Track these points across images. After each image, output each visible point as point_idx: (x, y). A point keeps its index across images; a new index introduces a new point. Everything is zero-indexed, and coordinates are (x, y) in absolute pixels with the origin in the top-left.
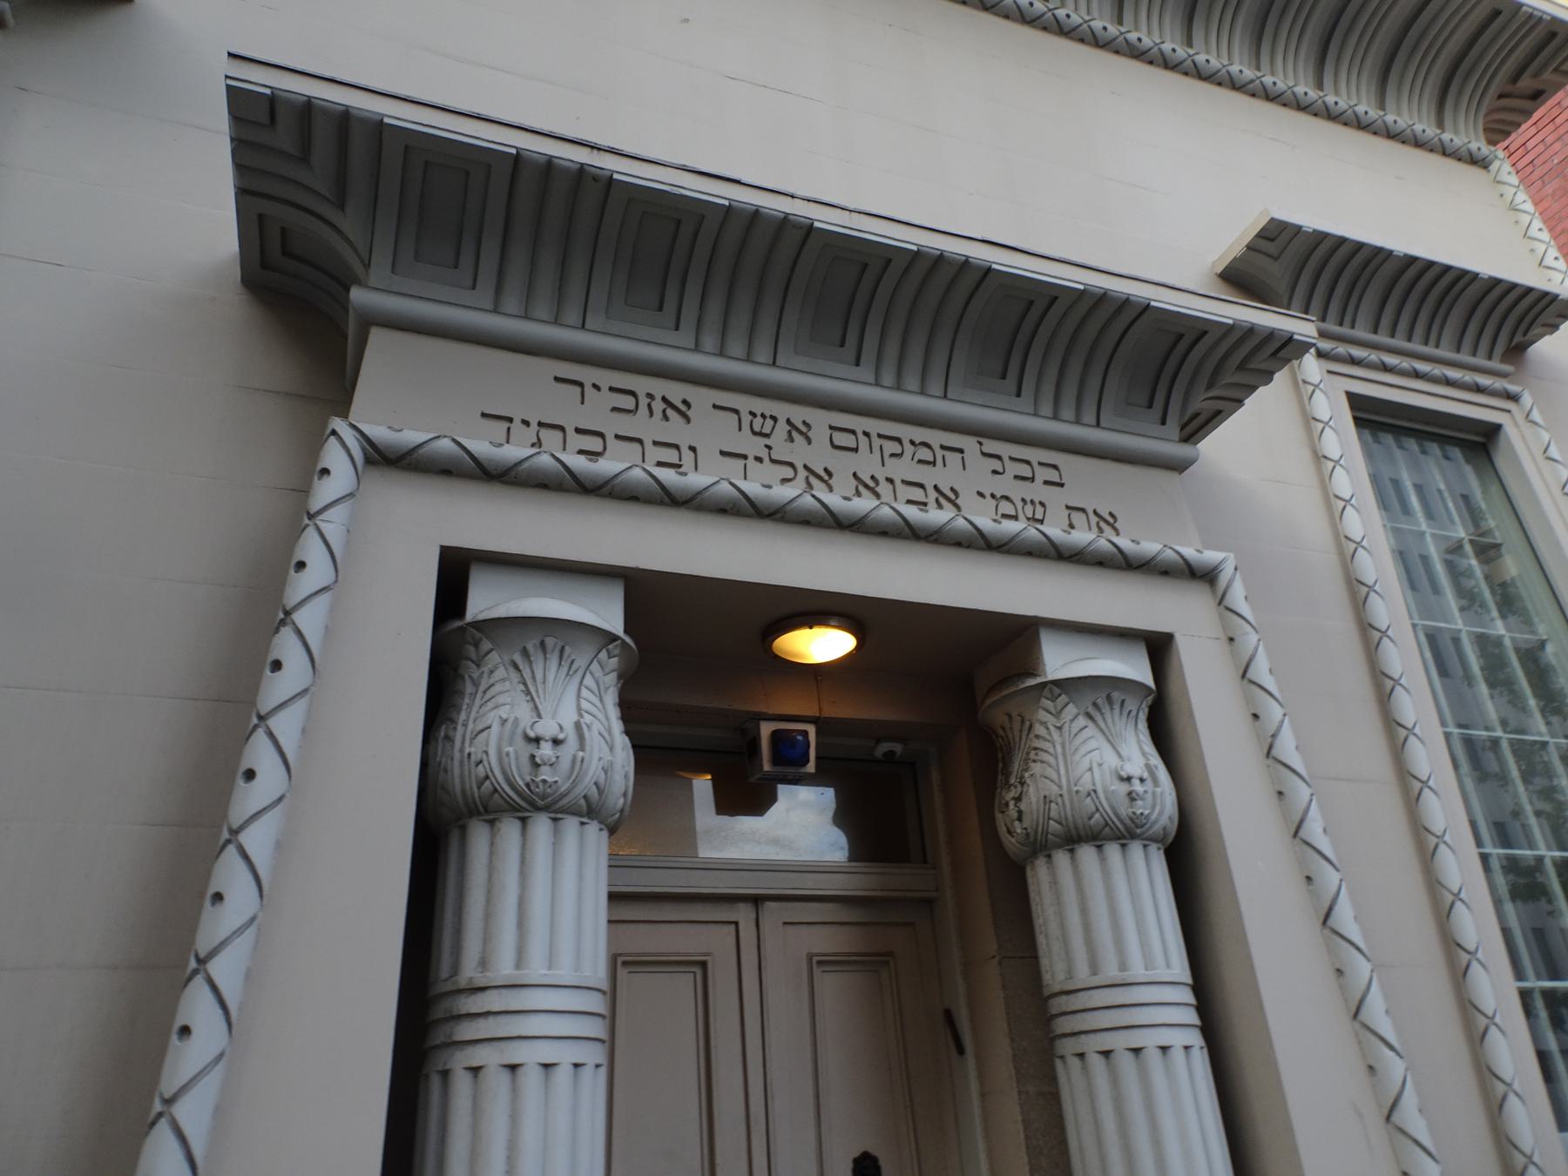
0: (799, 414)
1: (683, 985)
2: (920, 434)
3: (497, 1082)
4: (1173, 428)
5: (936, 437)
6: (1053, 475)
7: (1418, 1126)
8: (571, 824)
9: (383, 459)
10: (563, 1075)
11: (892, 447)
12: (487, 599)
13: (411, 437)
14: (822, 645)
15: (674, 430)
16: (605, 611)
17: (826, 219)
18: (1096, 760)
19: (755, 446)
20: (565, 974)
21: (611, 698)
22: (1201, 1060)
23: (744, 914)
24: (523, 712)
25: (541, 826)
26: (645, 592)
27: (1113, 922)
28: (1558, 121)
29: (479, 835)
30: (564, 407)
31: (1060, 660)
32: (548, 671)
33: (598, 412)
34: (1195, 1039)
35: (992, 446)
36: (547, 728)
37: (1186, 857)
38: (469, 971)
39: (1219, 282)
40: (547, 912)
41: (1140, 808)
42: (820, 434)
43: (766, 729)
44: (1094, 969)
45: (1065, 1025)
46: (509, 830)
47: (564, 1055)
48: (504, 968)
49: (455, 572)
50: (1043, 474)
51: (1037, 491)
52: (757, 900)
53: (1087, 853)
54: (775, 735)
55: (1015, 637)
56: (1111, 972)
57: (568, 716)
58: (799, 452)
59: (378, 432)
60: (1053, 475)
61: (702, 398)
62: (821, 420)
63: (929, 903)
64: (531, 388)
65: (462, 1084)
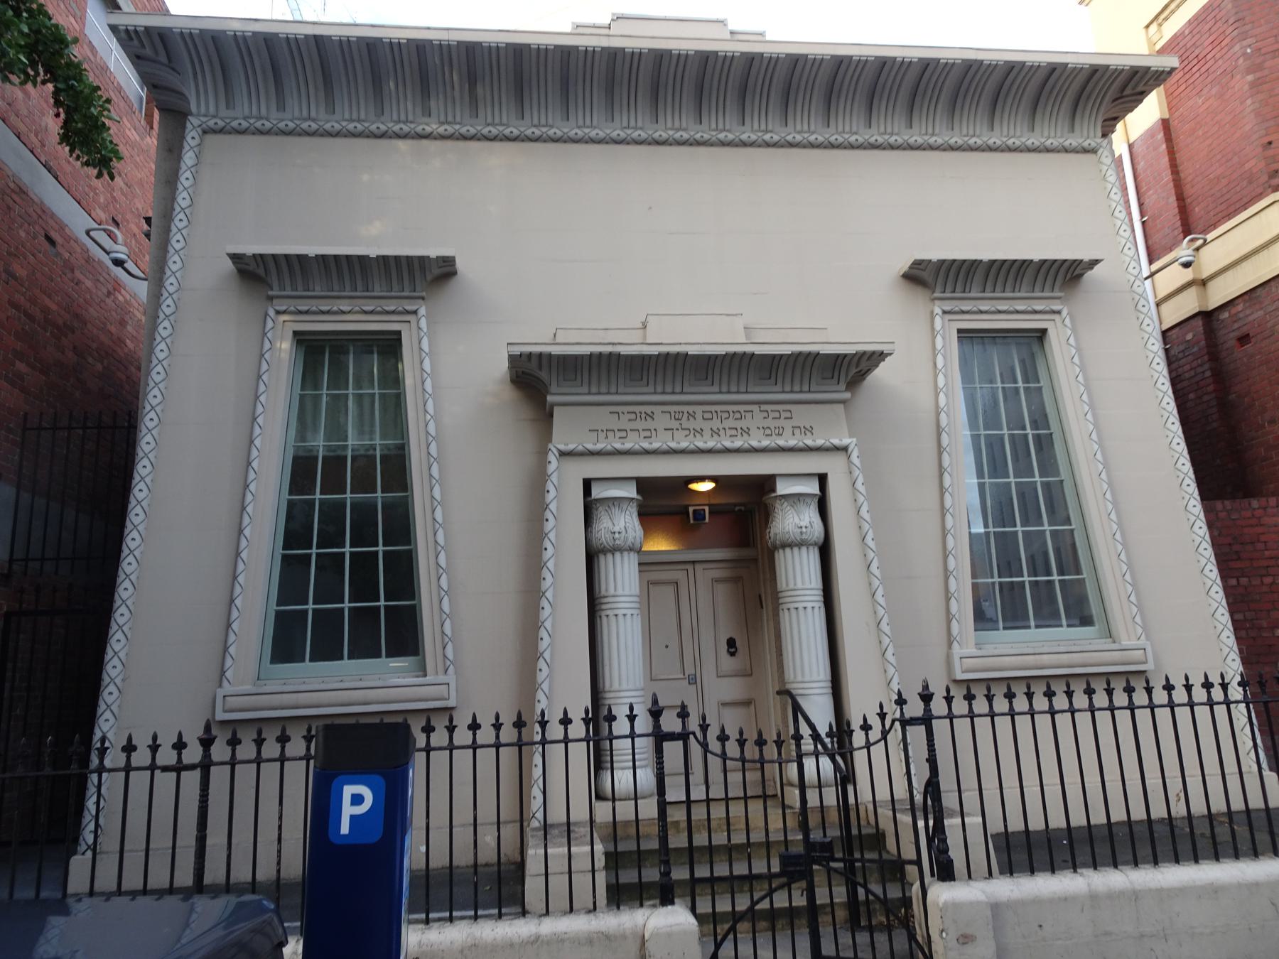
0: (691, 409)
1: (671, 589)
2: (736, 408)
3: (613, 619)
4: (843, 386)
5: (742, 408)
6: (788, 415)
7: (886, 628)
8: (626, 554)
9: (563, 454)
10: (628, 617)
11: (726, 415)
12: (597, 492)
13: (571, 447)
14: (707, 486)
15: (650, 424)
16: (630, 491)
17: (692, 350)
18: (794, 521)
19: (675, 424)
20: (627, 592)
21: (635, 515)
22: (823, 610)
23: (690, 567)
24: (610, 524)
25: (618, 555)
26: (644, 485)
27: (799, 572)
28: (1223, 44)
29: (602, 558)
30: (613, 423)
31: (783, 488)
32: (616, 511)
33: (624, 423)
34: (822, 605)
35: (764, 407)
36: (616, 529)
37: (825, 551)
38: (603, 593)
39: (902, 281)
40: (623, 578)
41: (804, 537)
42: (699, 416)
43: (691, 509)
44: (803, 583)
45: (781, 601)
46: (609, 556)
47: (629, 612)
48: (612, 591)
49: (587, 484)
50: (784, 415)
51: (782, 422)
52: (694, 562)
53: (788, 550)
54: (695, 511)
55: (764, 484)
56: (791, 586)
57: (622, 524)
58: (692, 424)
59: (562, 447)
60: (788, 415)
61: (657, 410)
62: (699, 410)
63: (755, 560)
64: (602, 417)
65: (604, 619)
